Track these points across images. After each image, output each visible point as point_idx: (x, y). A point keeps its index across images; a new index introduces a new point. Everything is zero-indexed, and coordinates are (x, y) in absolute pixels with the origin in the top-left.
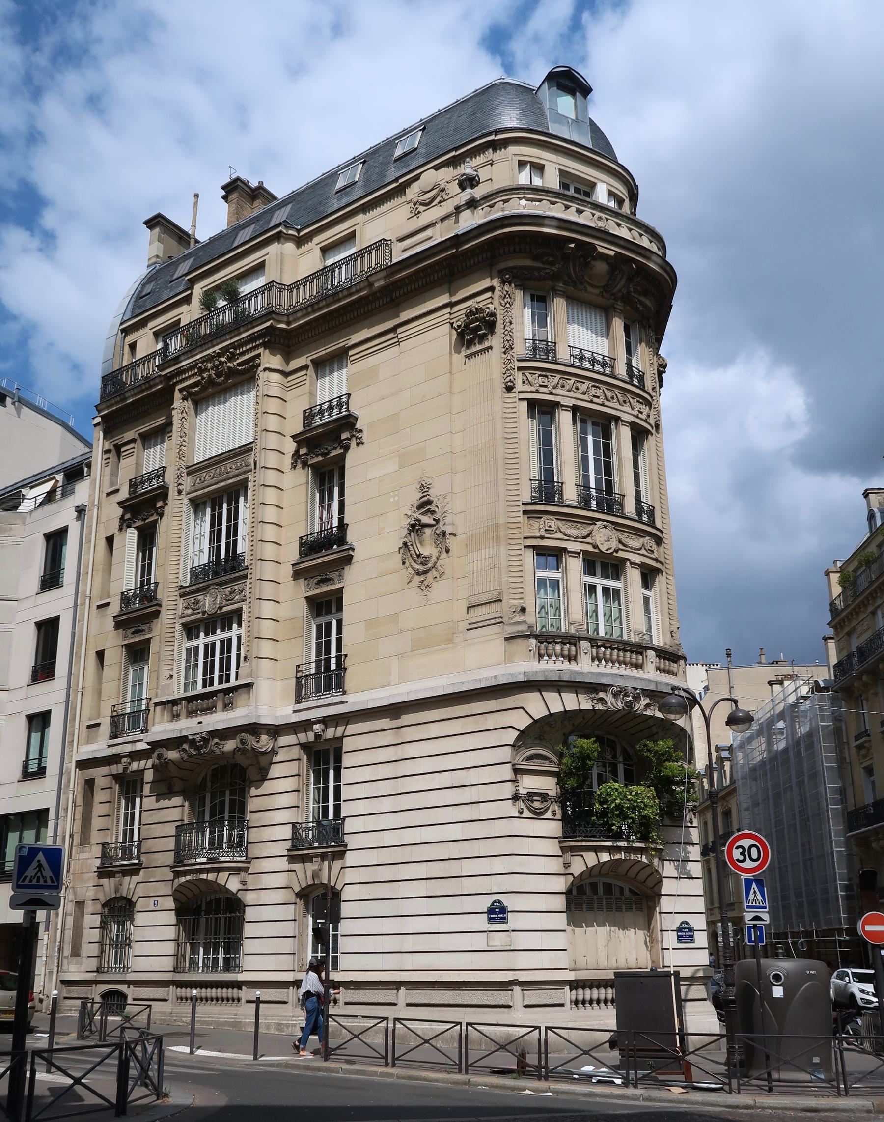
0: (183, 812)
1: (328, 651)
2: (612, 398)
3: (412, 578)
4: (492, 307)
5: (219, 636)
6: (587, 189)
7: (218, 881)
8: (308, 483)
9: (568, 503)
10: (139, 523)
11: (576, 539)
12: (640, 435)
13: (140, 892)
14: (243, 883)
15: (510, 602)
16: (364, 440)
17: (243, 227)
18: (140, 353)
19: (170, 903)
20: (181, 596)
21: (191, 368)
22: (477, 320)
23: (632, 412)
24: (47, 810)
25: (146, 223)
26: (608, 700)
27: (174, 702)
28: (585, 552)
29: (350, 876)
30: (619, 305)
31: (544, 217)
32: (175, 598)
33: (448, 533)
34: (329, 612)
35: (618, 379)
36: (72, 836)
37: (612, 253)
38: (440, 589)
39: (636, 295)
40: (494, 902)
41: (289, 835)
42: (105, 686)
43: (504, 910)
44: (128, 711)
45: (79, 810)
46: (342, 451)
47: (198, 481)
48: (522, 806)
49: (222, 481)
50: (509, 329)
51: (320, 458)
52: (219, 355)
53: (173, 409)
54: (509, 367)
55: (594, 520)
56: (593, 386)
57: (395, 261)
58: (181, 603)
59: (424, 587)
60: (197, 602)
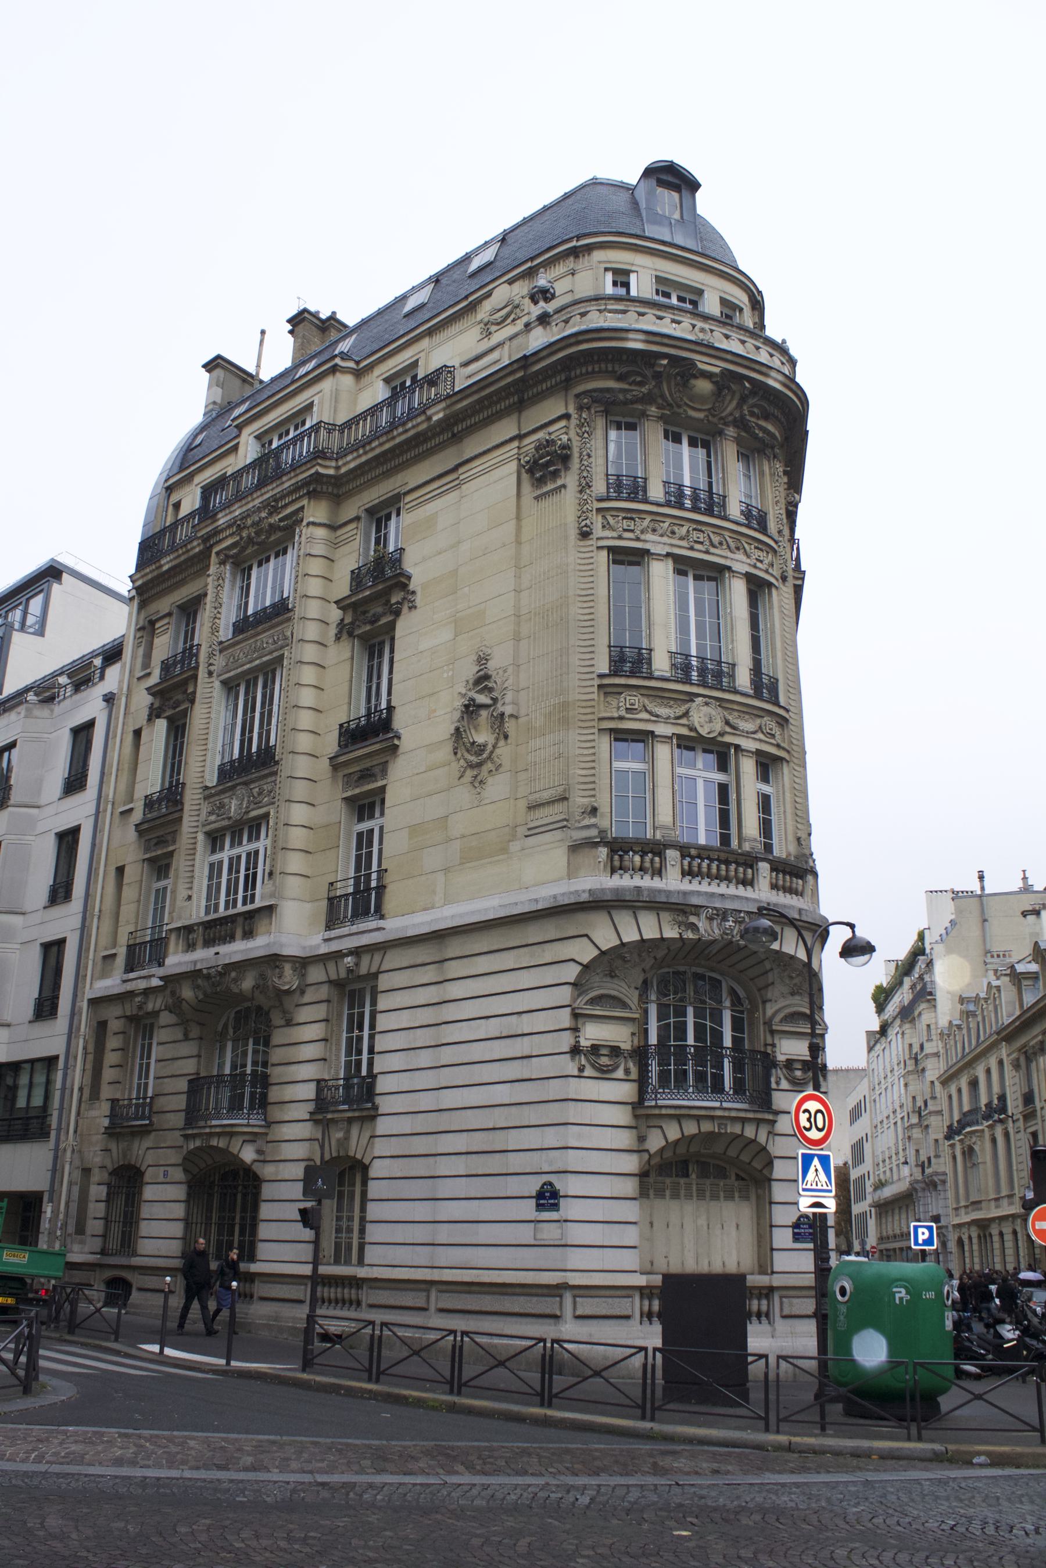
0: (199, 1063)
1: (369, 866)
2: (721, 544)
3: (464, 772)
4: (565, 438)
5: (246, 847)
6: (692, 296)
7: (231, 1149)
8: (352, 658)
9: (657, 674)
10: (169, 713)
11: (667, 720)
12: (758, 588)
13: (150, 1159)
14: (259, 1152)
15: (579, 800)
16: (418, 603)
17: (303, 363)
18: (184, 511)
19: (178, 1174)
20: (205, 799)
21: (229, 526)
22: (548, 454)
23: (748, 561)
24: (57, 1057)
25: (204, 366)
26: (700, 925)
27: (188, 929)
28: (679, 737)
29: (380, 1147)
30: (731, 431)
31: (627, 331)
32: (198, 802)
33: (507, 714)
34: (371, 816)
35: (729, 520)
36: (81, 1089)
37: (717, 370)
38: (497, 786)
39: (753, 419)
40: (545, 1184)
41: (312, 1095)
42: (124, 908)
43: (555, 1194)
44: (148, 938)
45: (90, 1057)
46: (391, 618)
47: (231, 660)
48: (583, 1061)
49: (256, 659)
50: (586, 463)
51: (368, 627)
52: (259, 510)
53: (209, 576)
54: (585, 509)
55: (691, 697)
56: (694, 529)
57: (457, 389)
58: (205, 808)
59: (477, 783)
60: (222, 806)
